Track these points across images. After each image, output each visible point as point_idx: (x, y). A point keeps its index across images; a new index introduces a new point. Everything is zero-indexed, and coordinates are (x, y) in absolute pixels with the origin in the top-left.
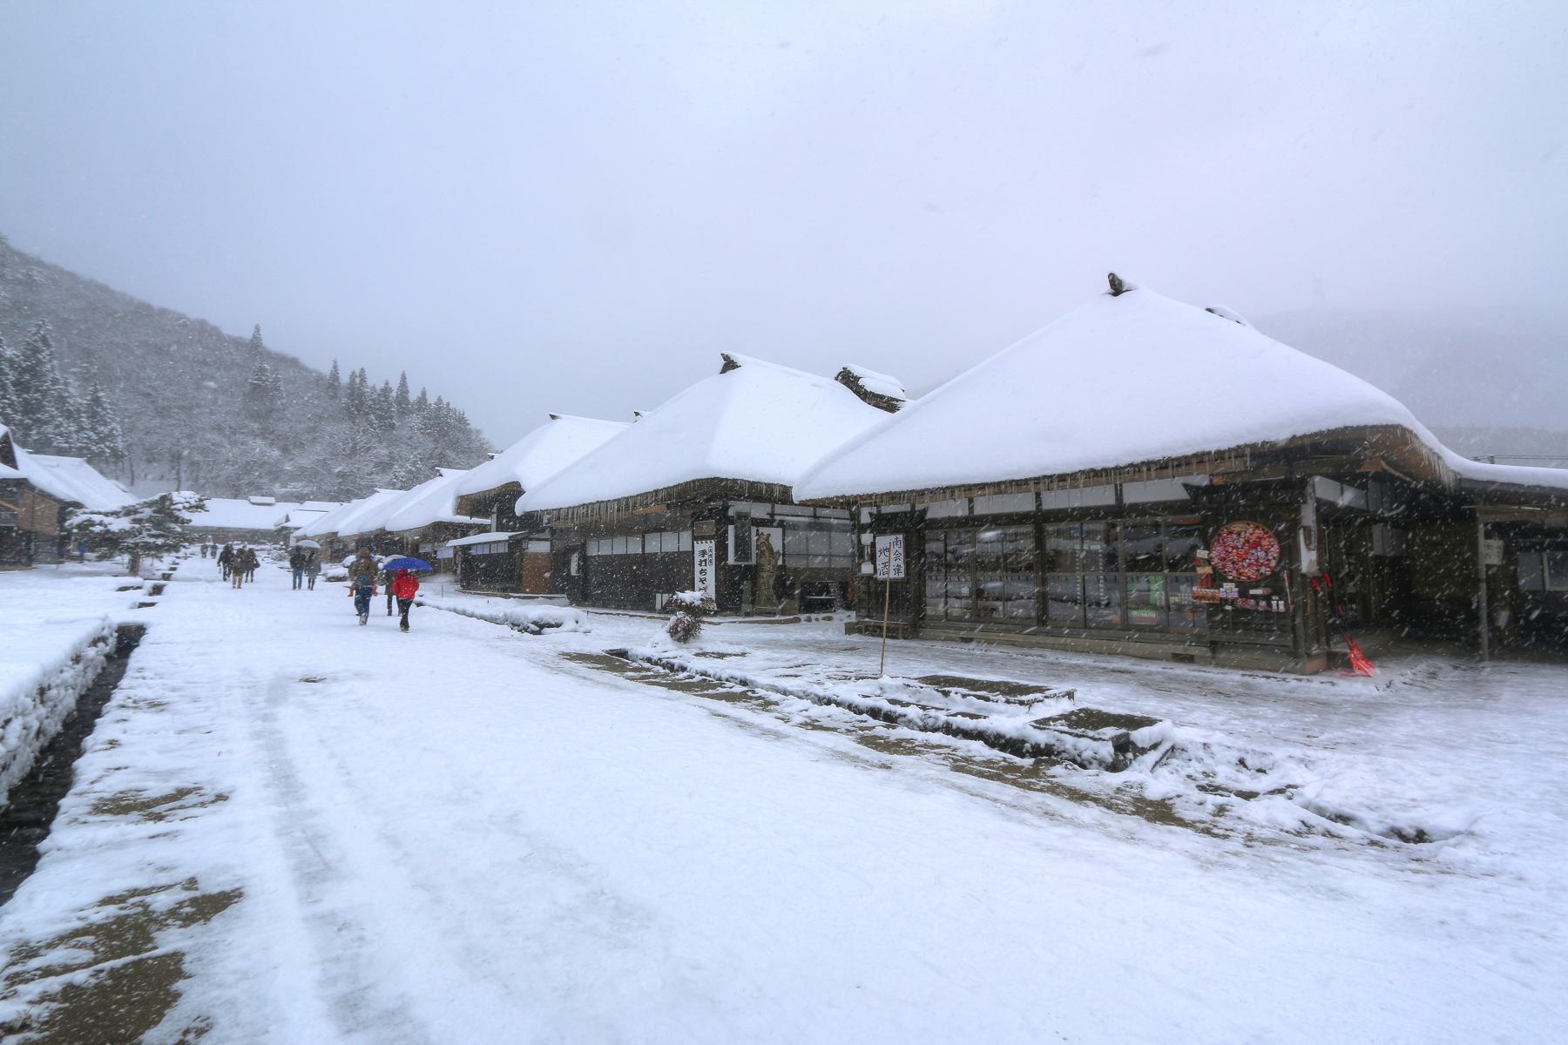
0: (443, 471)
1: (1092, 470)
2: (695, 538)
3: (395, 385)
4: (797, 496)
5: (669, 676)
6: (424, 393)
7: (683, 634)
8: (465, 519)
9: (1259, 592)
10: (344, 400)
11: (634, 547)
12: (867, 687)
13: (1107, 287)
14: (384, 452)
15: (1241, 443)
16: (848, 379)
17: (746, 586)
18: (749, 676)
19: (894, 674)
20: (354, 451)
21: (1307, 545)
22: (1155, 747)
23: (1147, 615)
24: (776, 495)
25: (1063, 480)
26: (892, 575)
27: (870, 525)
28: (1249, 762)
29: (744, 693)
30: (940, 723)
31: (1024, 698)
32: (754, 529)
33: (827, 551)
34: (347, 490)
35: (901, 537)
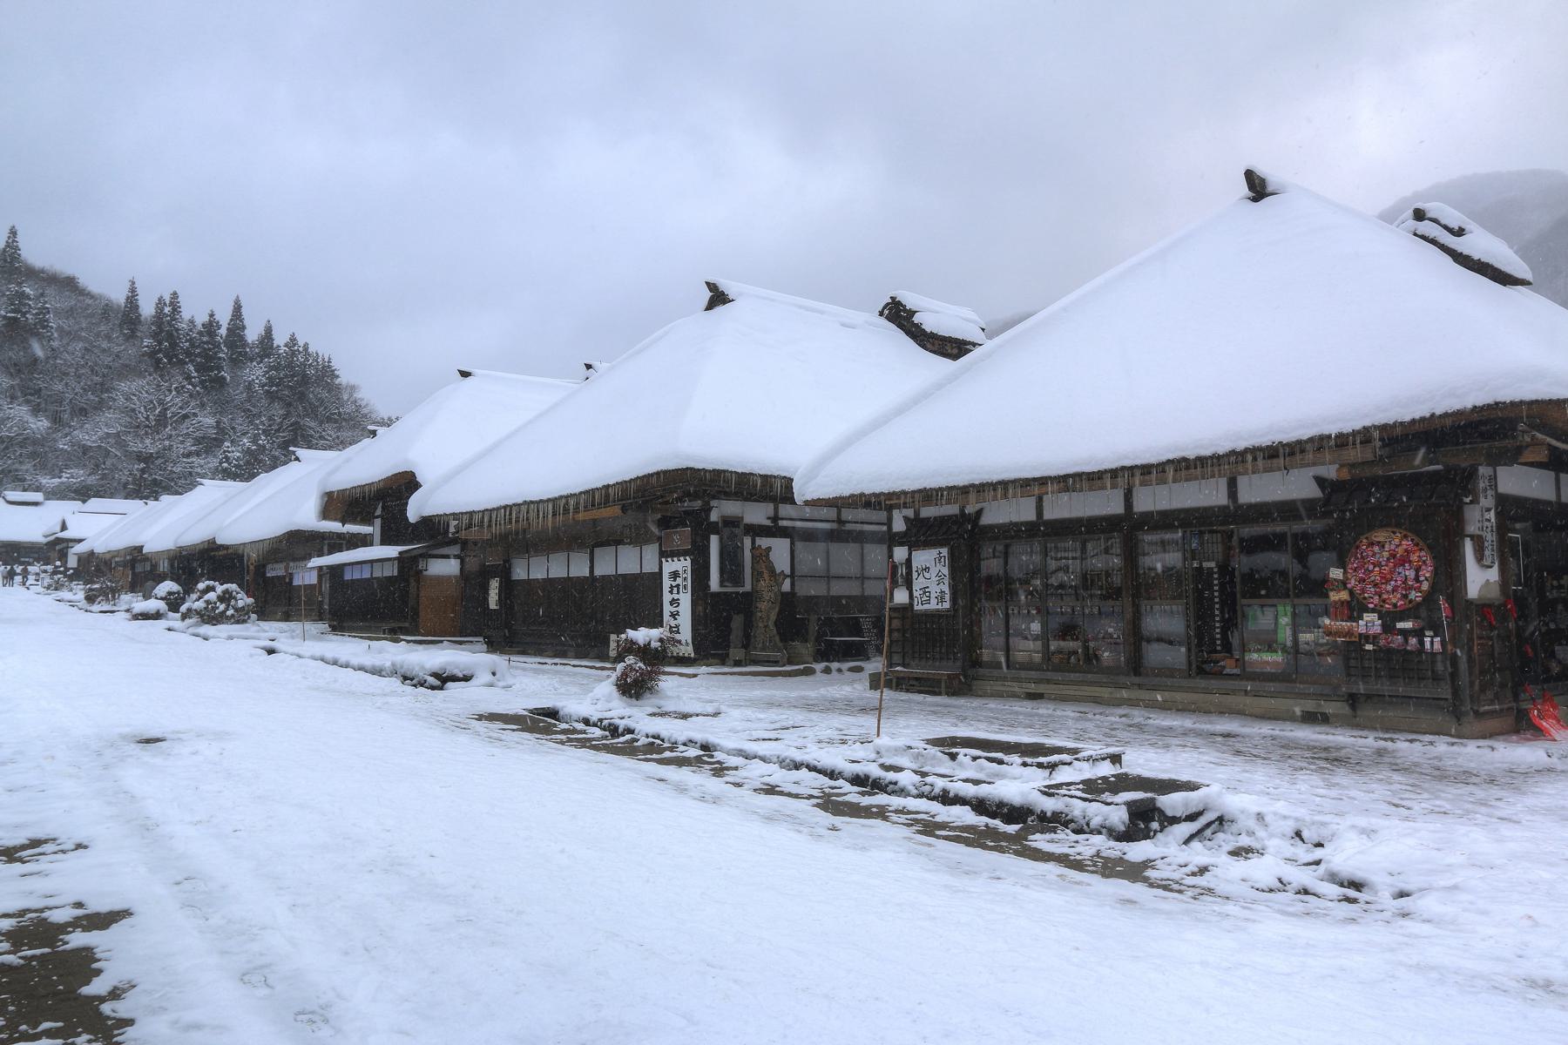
0: (300, 452)
1: (1184, 459)
3: (224, 318)
4: (804, 491)
5: (616, 740)
6: (269, 330)
7: (633, 688)
8: (334, 526)
9: (1408, 625)
10: (146, 342)
12: (859, 752)
13: (1244, 190)
14: (210, 421)
15: (1368, 423)
16: (898, 314)
17: (737, 622)
18: (712, 739)
19: (900, 733)
20: (162, 421)
21: (1480, 558)
22: (1192, 817)
23: (1274, 659)
24: (774, 489)
25: (1146, 471)
26: (933, 605)
28: (1305, 834)
29: (706, 757)
30: (937, 791)
31: (1041, 759)
32: (747, 541)
33: (846, 570)
35: (945, 551)
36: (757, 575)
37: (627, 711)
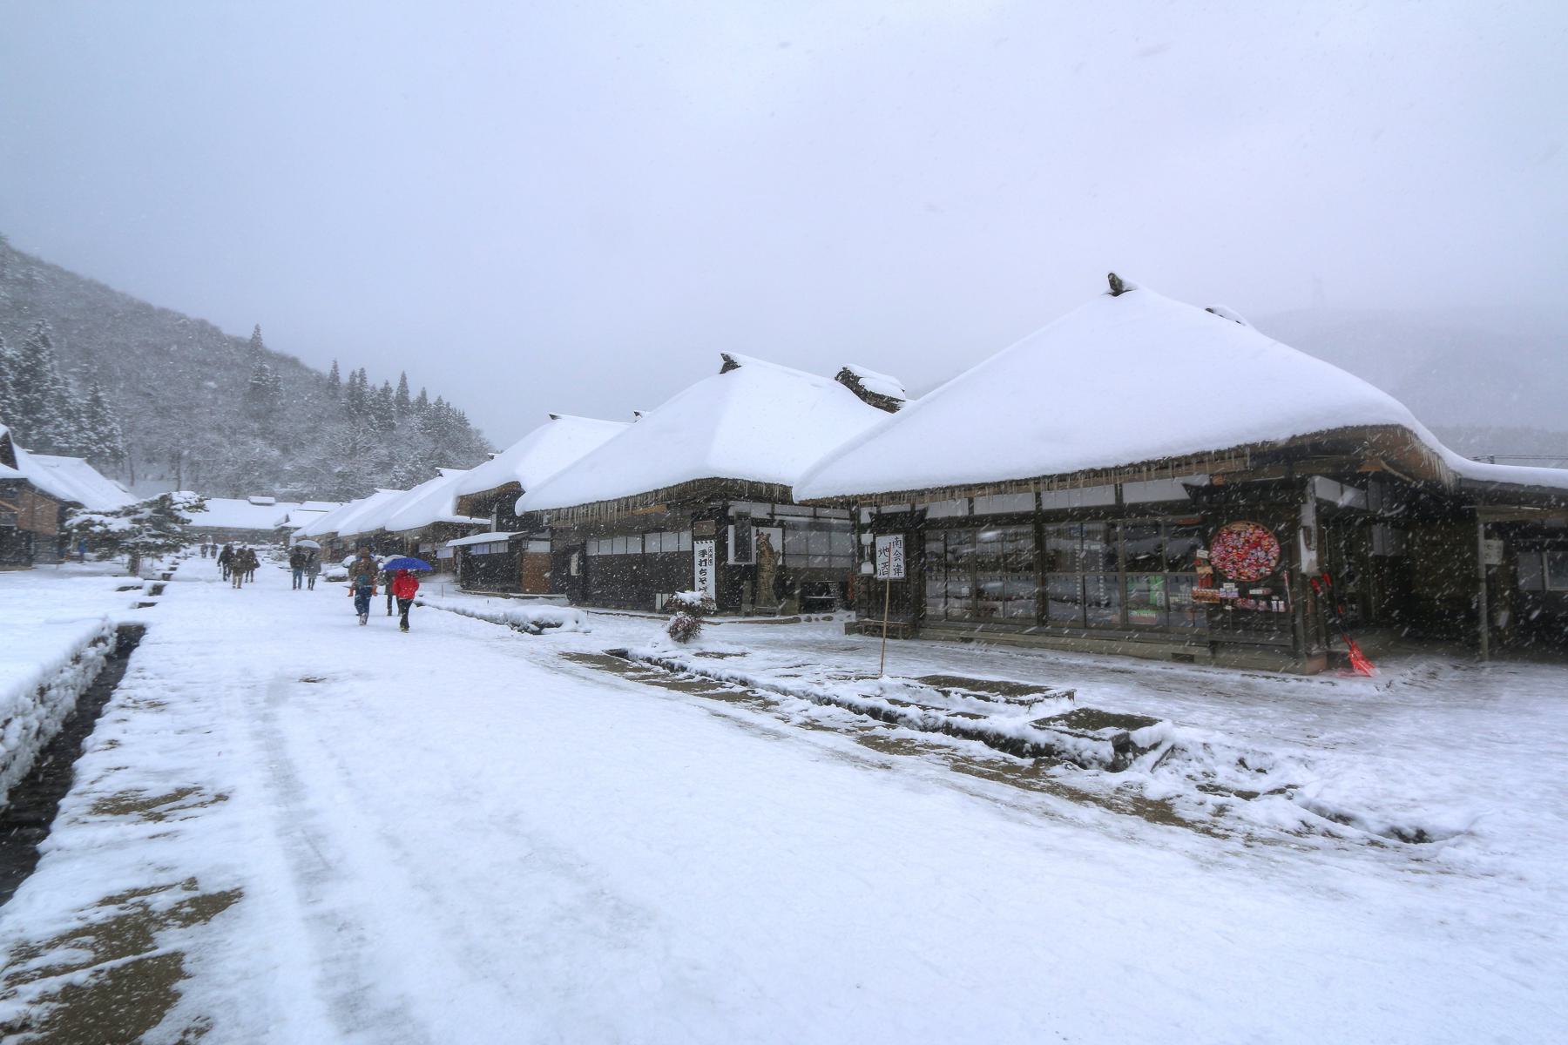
0: (443, 471)
1: (1092, 470)
2: (695, 538)
3: (395, 385)
4: (798, 495)
5: (670, 676)
6: (424, 393)
7: (683, 634)
8: (466, 519)
9: (1259, 592)
11: (634, 547)
12: (867, 687)
13: (1107, 287)
14: (385, 452)
15: (1241, 443)
16: (848, 379)
17: (746, 586)
18: (749, 676)
19: (894, 674)
21: (1307, 546)
22: (1155, 747)
23: (1147, 615)
24: (776, 495)
25: (1063, 480)
26: (892, 575)
27: (870, 525)
28: (1249, 762)
29: (744, 693)
30: (940, 723)
31: (1024, 698)
32: (754, 529)
33: (827, 551)
34: (347, 490)
35: (901, 537)
36: (760, 555)
37: (679, 653)
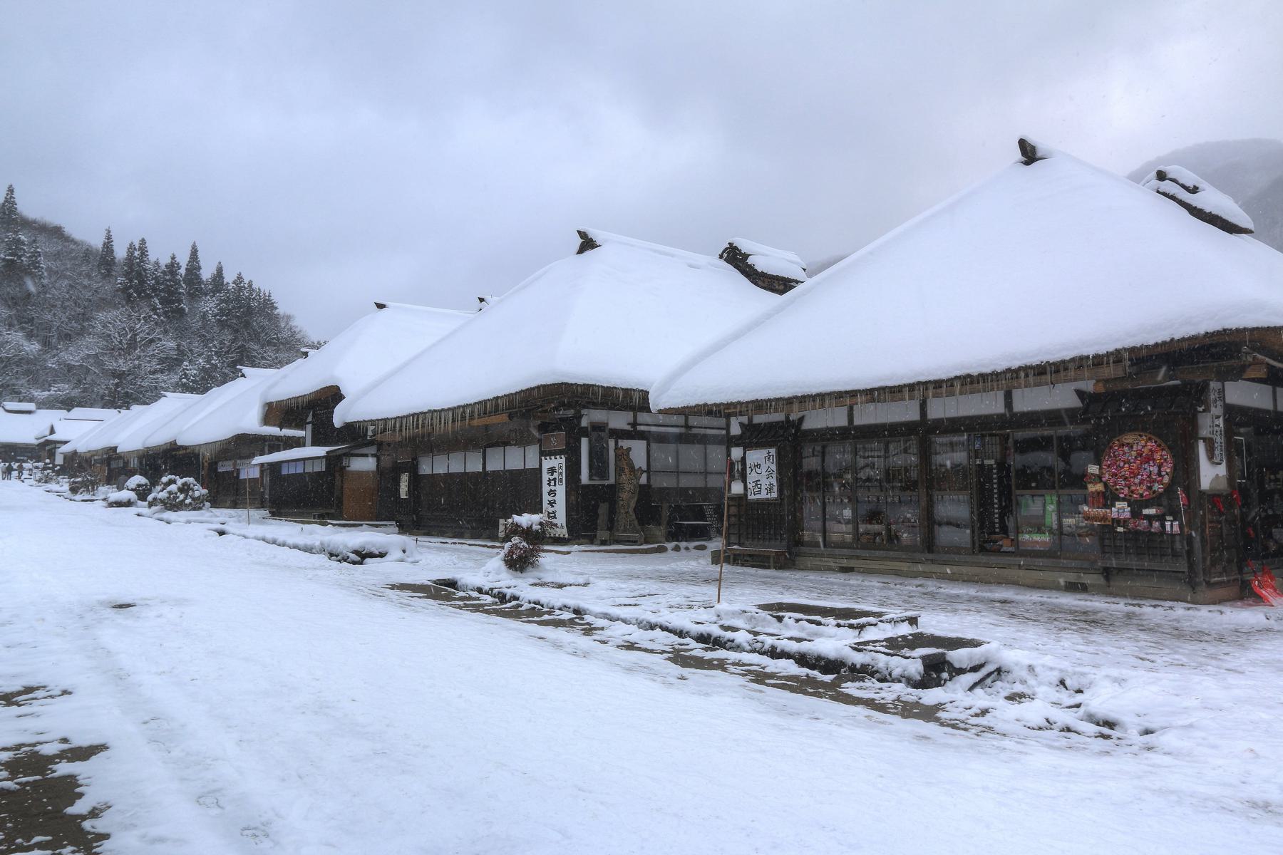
0: (246, 370)
1: (969, 376)
2: (543, 453)
3: (183, 260)
4: (658, 401)
5: (504, 606)
6: (220, 270)
7: (518, 563)
8: (274, 431)
9: (1152, 511)
10: (120, 280)
11: (474, 464)
12: (703, 615)
13: (1018, 155)
14: (172, 344)
15: (1119, 346)
16: (735, 257)
17: (603, 509)
18: (583, 605)
19: (736, 600)
20: (132, 344)
21: (1211, 456)
22: (975, 669)
24: (634, 400)
25: (938, 386)
26: (764, 495)
27: (740, 437)
28: (1068, 683)
29: (577, 619)
30: (767, 647)
31: (852, 621)
32: (612, 443)
33: (693, 466)
34: (124, 394)
35: (773, 451)
36: (619, 471)
